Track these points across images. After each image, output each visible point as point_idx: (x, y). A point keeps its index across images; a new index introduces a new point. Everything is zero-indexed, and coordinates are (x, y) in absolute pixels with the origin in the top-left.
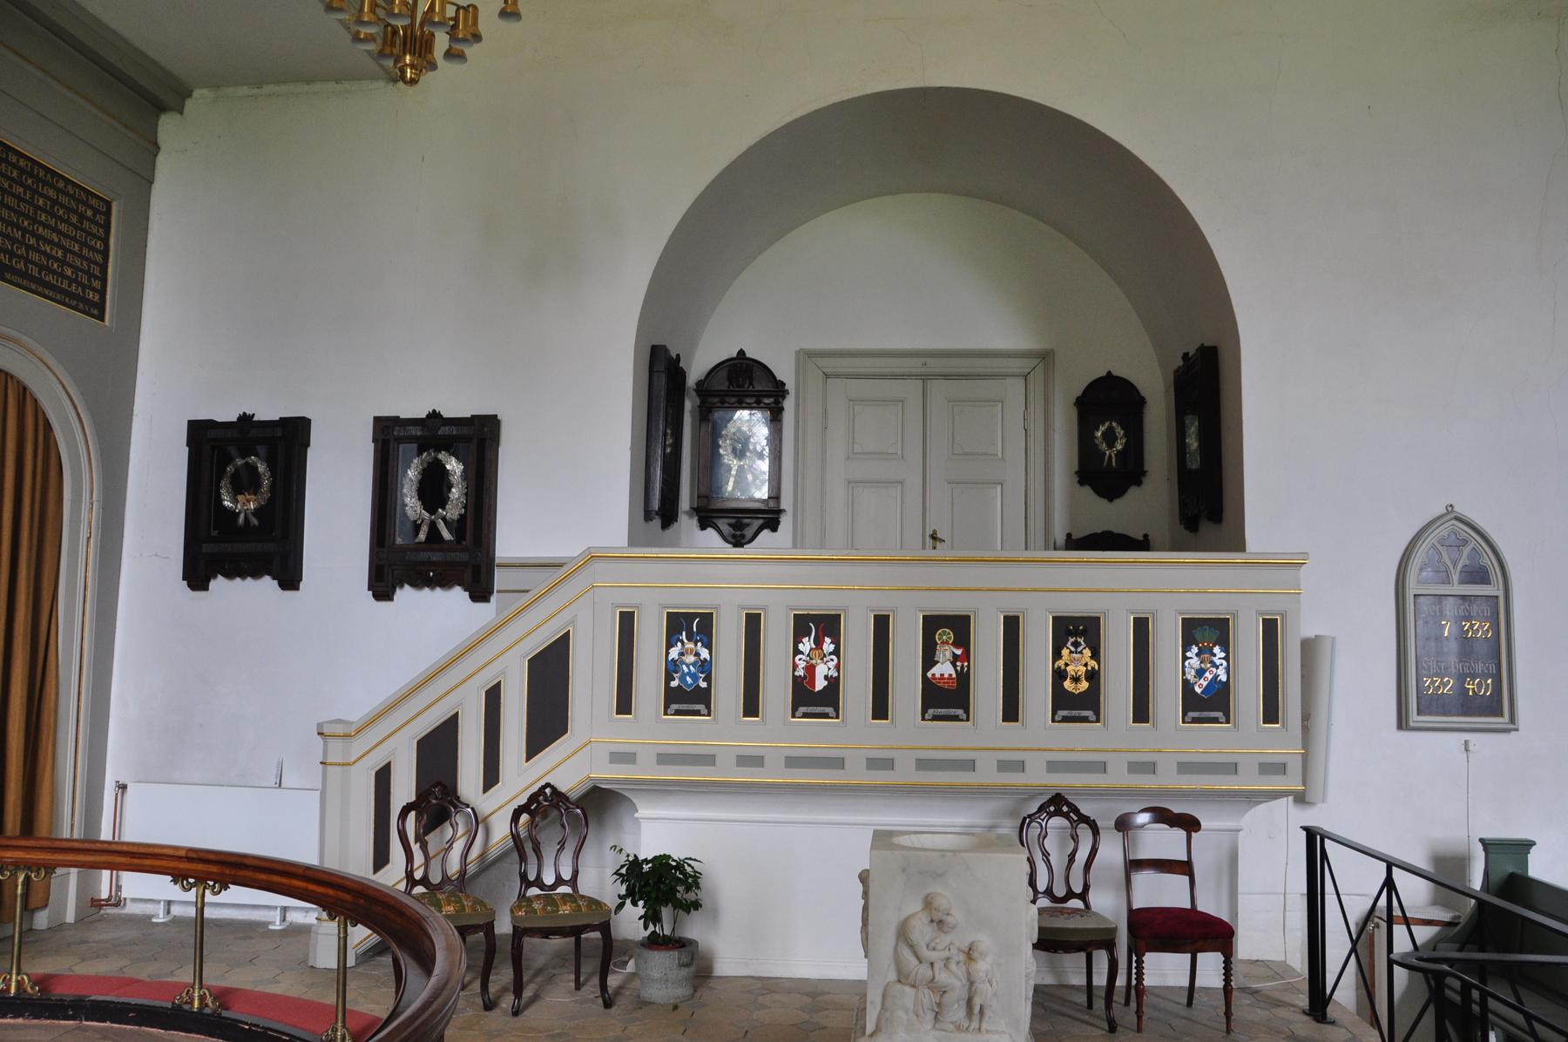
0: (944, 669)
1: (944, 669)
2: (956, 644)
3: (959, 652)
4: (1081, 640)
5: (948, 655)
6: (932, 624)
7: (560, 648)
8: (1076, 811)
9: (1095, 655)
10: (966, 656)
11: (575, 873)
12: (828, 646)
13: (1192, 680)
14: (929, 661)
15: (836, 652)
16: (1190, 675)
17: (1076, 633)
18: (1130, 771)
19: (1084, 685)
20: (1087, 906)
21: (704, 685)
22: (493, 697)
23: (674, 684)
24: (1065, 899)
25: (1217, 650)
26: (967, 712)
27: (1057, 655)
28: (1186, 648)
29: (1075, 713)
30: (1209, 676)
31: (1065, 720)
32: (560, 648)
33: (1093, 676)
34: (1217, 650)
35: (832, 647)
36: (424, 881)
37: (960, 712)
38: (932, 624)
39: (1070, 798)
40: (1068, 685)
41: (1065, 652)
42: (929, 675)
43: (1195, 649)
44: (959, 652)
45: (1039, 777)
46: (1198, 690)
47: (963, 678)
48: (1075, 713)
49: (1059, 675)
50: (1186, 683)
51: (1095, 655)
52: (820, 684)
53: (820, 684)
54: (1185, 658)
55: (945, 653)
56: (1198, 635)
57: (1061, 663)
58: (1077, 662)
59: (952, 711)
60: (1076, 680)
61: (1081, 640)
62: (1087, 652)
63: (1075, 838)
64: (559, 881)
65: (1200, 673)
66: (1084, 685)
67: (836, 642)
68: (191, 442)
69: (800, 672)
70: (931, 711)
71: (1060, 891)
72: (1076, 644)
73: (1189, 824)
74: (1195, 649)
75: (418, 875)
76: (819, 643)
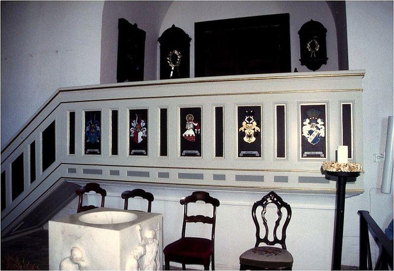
0: (190, 132)
1: (190, 132)
2: (195, 121)
3: (196, 125)
4: (252, 118)
5: (191, 126)
6: (185, 112)
7: (52, 126)
8: (279, 199)
9: (259, 125)
10: (199, 126)
11: (284, 237)
12: (143, 124)
13: (307, 136)
14: (183, 129)
15: (146, 126)
16: (306, 134)
17: (249, 114)
18: (236, 180)
19: (253, 139)
20: (284, 248)
21: (98, 141)
22: (33, 146)
23: (88, 141)
24: (273, 243)
25: (319, 121)
26: (147, 151)
27: (240, 125)
28: (303, 119)
29: (313, 153)
30: (315, 134)
31: (245, 156)
32: (52, 126)
33: (257, 135)
34: (319, 121)
35: (144, 124)
36: (266, 240)
37: (197, 152)
38: (185, 112)
39: (278, 194)
40: (246, 139)
41: (244, 123)
42: (183, 135)
43: (308, 121)
44: (196, 125)
45: (270, 183)
46: (310, 141)
47: (198, 137)
48: (313, 153)
49: (242, 135)
50: (303, 137)
51: (259, 125)
52: (140, 140)
53: (140, 140)
54: (303, 125)
55: (190, 125)
56: (309, 113)
57: (242, 129)
58: (250, 128)
59: (193, 152)
60: (250, 136)
61: (252, 118)
62: (255, 123)
63: (280, 213)
64: (276, 241)
65: (311, 132)
66: (253, 139)
67: (146, 122)
68: (286, 14)
69: (132, 135)
70: (184, 152)
71: (271, 238)
72: (249, 120)
73: (216, 203)
74: (308, 121)
75: (262, 236)
76: (139, 122)
